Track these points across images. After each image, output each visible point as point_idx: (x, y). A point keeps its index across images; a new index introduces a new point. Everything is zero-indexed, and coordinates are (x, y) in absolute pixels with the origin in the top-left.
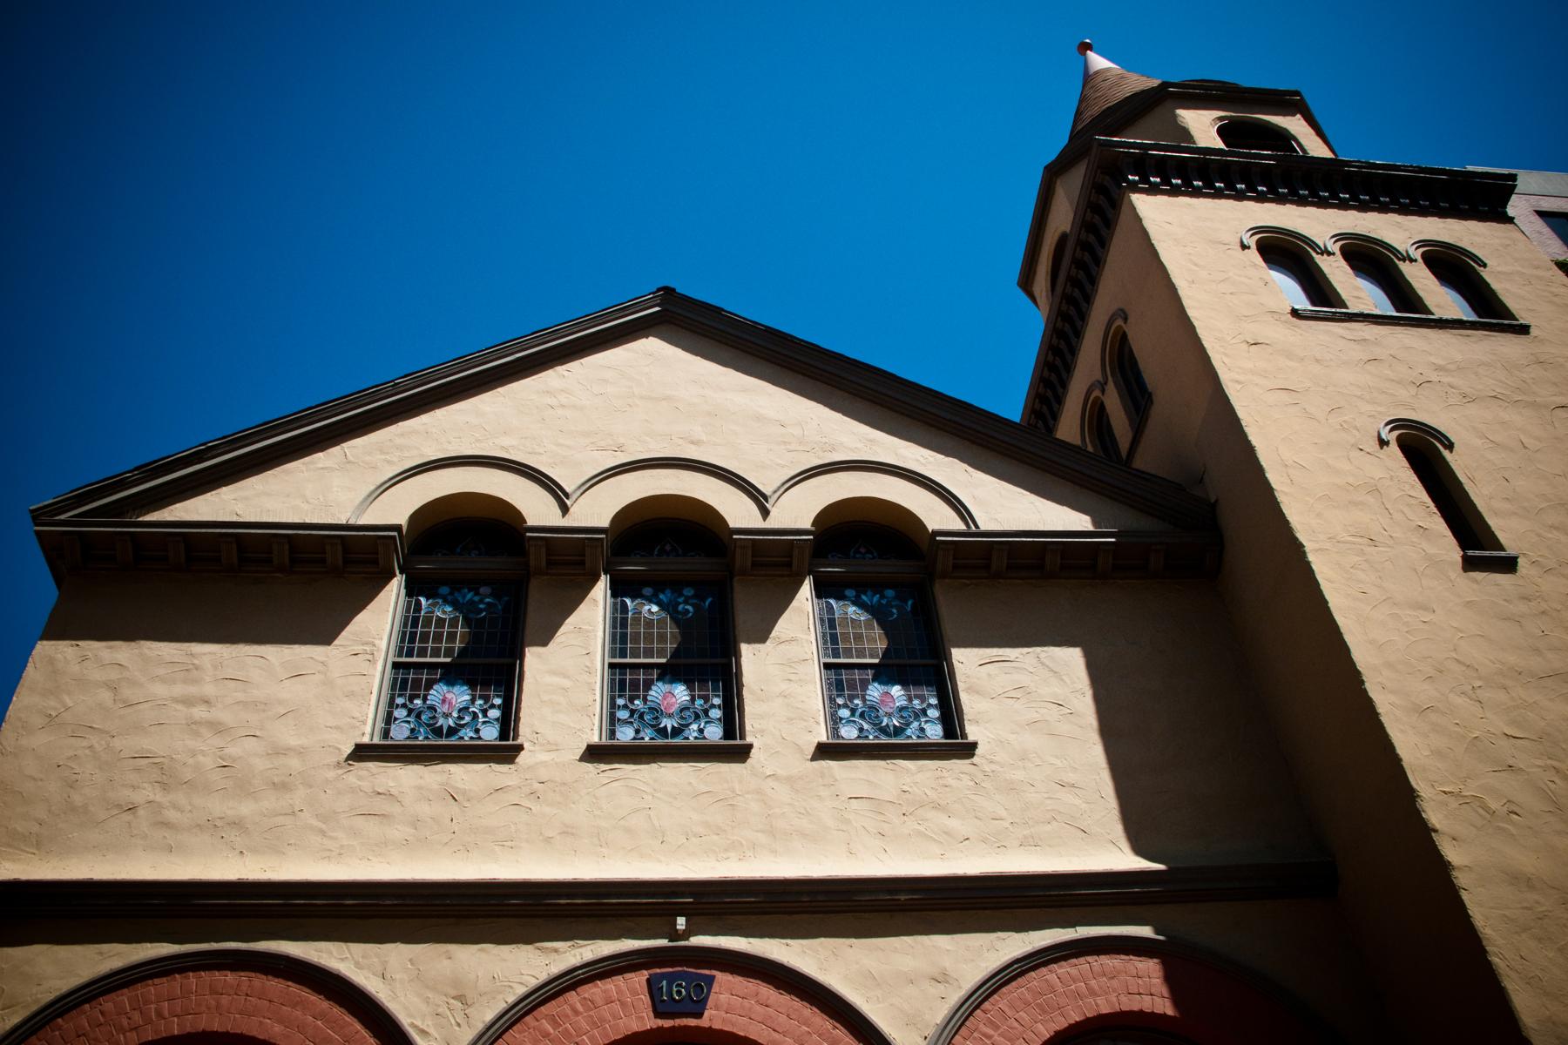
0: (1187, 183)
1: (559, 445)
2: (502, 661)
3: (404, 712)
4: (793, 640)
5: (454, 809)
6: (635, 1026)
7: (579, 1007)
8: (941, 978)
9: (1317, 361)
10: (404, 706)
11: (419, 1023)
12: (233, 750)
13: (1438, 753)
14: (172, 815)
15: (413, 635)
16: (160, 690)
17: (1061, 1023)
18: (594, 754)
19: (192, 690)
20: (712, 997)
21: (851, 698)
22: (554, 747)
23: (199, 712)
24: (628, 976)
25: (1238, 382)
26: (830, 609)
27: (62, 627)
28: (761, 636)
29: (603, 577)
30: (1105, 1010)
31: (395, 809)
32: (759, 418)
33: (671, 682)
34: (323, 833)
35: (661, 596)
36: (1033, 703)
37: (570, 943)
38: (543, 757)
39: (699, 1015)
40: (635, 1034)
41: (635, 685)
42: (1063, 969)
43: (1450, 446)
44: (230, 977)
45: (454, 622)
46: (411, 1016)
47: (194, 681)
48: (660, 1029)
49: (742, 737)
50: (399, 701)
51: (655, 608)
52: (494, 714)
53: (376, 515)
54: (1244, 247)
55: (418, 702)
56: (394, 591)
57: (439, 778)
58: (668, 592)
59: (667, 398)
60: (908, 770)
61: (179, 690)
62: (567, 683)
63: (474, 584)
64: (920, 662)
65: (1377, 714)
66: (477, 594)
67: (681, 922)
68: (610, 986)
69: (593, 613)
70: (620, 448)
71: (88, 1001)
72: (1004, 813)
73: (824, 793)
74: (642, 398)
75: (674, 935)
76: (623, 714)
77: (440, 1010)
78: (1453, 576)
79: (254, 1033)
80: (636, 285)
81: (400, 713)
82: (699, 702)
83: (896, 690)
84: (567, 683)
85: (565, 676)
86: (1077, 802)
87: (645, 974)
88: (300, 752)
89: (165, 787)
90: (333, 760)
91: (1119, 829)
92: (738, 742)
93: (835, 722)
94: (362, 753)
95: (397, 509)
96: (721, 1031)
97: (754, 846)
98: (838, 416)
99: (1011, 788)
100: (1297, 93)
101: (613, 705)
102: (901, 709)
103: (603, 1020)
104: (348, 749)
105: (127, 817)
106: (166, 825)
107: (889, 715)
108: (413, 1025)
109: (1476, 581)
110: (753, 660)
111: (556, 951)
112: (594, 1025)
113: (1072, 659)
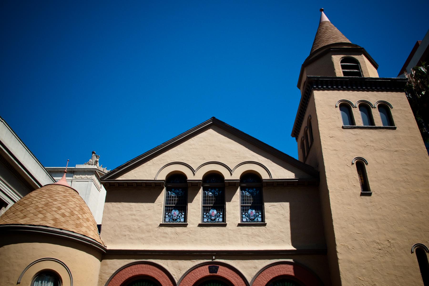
1: (193, 158)
4: (235, 201)
5: (177, 235)
6: (206, 275)
8: (256, 268)
9: (344, 141)
12: (140, 225)
13: (343, 237)
14: (132, 237)
16: (126, 213)
17: (274, 276)
18: (200, 225)
19: (132, 213)
21: (245, 213)
22: (193, 224)
23: (133, 217)
25: (326, 149)
26: (243, 193)
28: (230, 201)
30: (282, 274)
31: (167, 236)
34: (156, 240)
36: (278, 213)
38: (192, 226)
39: (216, 273)
41: (207, 210)
42: (276, 267)
43: (367, 164)
44: (144, 265)
45: (175, 197)
47: (132, 211)
50: (167, 214)
51: (211, 193)
52: (183, 216)
53: (159, 178)
54: (336, 107)
56: (164, 191)
59: (213, 146)
61: (130, 212)
62: (195, 211)
65: (333, 229)
67: (214, 257)
69: (199, 197)
70: (204, 159)
72: (270, 237)
73: (239, 233)
75: (213, 260)
76: (205, 216)
78: (358, 197)
81: (167, 216)
83: (254, 211)
84: (195, 211)
85: (195, 209)
86: (283, 235)
87: (208, 266)
88: (151, 225)
89: (130, 232)
90: (156, 226)
91: (290, 240)
94: (161, 225)
95: (162, 177)
97: (226, 243)
98: (247, 149)
99: (272, 232)
100: (363, 48)
101: (203, 214)
102: (254, 215)
104: (159, 225)
105: (125, 237)
106: (131, 239)
109: (362, 198)
110: (228, 205)
113: (287, 205)
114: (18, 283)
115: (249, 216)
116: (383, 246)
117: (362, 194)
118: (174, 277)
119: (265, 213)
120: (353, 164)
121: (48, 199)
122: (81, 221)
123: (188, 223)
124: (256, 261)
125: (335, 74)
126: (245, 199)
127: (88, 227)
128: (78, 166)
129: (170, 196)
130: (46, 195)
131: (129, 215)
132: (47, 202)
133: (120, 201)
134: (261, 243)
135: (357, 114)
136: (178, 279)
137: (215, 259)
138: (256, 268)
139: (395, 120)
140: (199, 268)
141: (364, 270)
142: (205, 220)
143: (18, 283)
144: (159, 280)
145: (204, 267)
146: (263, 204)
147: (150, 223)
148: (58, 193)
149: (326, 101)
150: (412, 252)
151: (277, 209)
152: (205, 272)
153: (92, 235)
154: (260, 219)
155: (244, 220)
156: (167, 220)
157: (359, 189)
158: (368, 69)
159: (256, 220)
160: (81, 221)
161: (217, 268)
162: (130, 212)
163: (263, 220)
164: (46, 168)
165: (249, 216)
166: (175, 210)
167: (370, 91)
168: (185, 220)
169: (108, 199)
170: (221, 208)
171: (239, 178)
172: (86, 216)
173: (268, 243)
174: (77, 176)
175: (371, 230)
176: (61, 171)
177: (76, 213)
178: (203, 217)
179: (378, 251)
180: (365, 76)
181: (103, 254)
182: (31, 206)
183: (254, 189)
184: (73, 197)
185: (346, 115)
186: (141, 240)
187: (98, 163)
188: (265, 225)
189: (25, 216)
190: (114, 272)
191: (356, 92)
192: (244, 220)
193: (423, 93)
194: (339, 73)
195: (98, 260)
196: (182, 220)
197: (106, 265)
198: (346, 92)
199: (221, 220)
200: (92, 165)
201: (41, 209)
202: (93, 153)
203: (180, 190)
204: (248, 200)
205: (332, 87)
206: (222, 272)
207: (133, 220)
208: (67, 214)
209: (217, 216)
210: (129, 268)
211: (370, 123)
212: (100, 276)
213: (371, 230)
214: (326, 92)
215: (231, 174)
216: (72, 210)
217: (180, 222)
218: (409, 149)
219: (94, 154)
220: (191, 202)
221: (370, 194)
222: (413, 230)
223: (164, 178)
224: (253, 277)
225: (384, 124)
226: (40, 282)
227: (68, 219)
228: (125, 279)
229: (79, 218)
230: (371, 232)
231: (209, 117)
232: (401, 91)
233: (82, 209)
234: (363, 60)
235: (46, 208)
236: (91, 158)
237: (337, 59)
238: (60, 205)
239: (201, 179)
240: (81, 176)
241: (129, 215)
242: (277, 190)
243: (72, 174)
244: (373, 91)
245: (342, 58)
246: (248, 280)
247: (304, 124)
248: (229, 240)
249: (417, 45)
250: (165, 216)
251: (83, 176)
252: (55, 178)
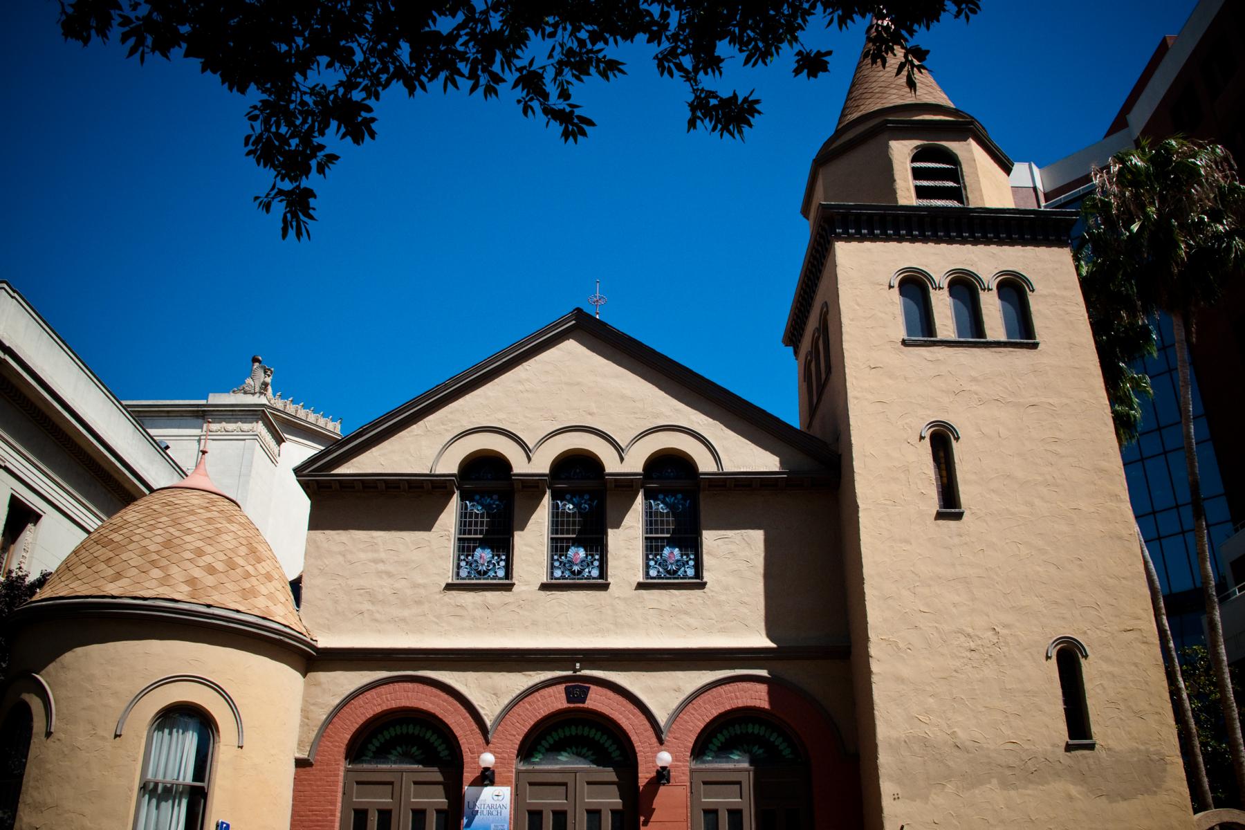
0: (871, 233)
5: (489, 613)
8: (678, 690)
9: (906, 378)
12: (397, 585)
14: (377, 616)
16: (362, 556)
17: (722, 710)
19: (376, 555)
22: (527, 583)
23: (381, 567)
32: (623, 397)
36: (736, 557)
38: (524, 588)
41: (562, 547)
43: (957, 439)
45: (482, 516)
47: (376, 551)
52: (502, 564)
53: (441, 469)
59: (578, 384)
61: (370, 555)
62: (532, 550)
67: (578, 665)
69: (542, 517)
76: (557, 564)
81: (463, 564)
84: (532, 550)
87: (564, 686)
88: (424, 586)
89: (373, 603)
91: (763, 624)
94: (449, 587)
95: (449, 465)
98: (662, 393)
99: (719, 604)
105: (360, 617)
106: (376, 620)
113: (758, 536)
114: (116, 736)
115: (663, 563)
116: (979, 642)
117: (940, 516)
118: (482, 712)
119: (705, 557)
120: (922, 438)
121: (171, 530)
122: (255, 582)
123: (514, 581)
124: (680, 674)
125: (894, 192)
126: (656, 521)
127: (270, 597)
128: (216, 399)
129: (471, 514)
130: (164, 519)
131: (370, 561)
132: (168, 536)
134: (692, 629)
135: (943, 306)
136: (493, 718)
138: (678, 690)
139: (1038, 323)
140: (543, 692)
141: (931, 700)
142: (558, 573)
143: (116, 736)
146: (700, 535)
147: (421, 581)
148: (192, 512)
149: (866, 272)
150: (1048, 658)
151: (733, 547)
152: (556, 700)
153: (282, 613)
154: (691, 572)
155: (653, 573)
156: (464, 573)
157: (933, 503)
158: (982, 180)
159: (680, 573)
160: (255, 582)
161: (585, 691)
162: (370, 555)
163: (698, 572)
164: (124, 403)
165: (663, 563)
166: (483, 548)
167: (981, 243)
168: (509, 574)
169: (316, 523)
170: (596, 544)
171: (640, 470)
172: (264, 567)
173: (709, 630)
174: (214, 427)
175: (955, 605)
176: (168, 412)
177: (240, 561)
178: (552, 567)
179: (969, 654)
180: (973, 203)
181: (311, 659)
182: (131, 547)
183: (679, 496)
184: (230, 521)
185: (914, 308)
186: (401, 623)
187: (270, 388)
188: (702, 586)
189: (118, 576)
190: (337, 701)
191: (943, 246)
192: (653, 573)
193: (1135, 228)
194: (906, 193)
195: (298, 675)
196: (501, 573)
197: (318, 684)
198: (918, 245)
199: (595, 573)
200: (254, 394)
201: (155, 557)
202: (255, 360)
203: (495, 497)
204: (662, 522)
205: (884, 232)
206: (597, 700)
207: (379, 573)
208: (220, 566)
209: (585, 563)
210: (373, 692)
211: (973, 331)
212: (305, 713)
213: (955, 605)
214: (867, 244)
215: (622, 459)
216: (230, 554)
217: (589, 578)
218: (1065, 401)
219: (257, 364)
221: (959, 516)
222: (1056, 603)
223: (454, 469)
224: (670, 712)
225: (1009, 336)
226: (167, 731)
227: (223, 578)
228: (364, 719)
229: (247, 576)
230: (954, 610)
231: (567, 309)
232: (1060, 243)
233: (253, 551)
234: (971, 154)
235: (166, 552)
236: (250, 374)
237: (902, 151)
238: (200, 544)
239: (547, 471)
240: (224, 424)
241: (370, 561)
242: (737, 498)
243: (200, 421)
244: (988, 242)
245: (916, 148)
247: (813, 323)
248: (616, 624)
249: (1163, 48)
251: (230, 426)
252: (152, 432)
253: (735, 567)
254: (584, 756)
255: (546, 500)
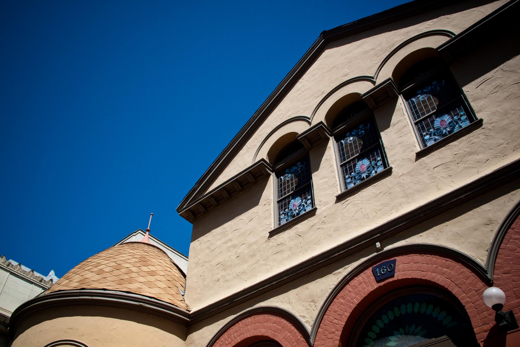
2: (376, 144)
3: (283, 215)
4: (399, 121)
6: (371, 289)
7: (351, 290)
10: (349, 177)
11: (302, 314)
14: (228, 277)
15: (281, 190)
16: (219, 243)
19: (227, 238)
20: (396, 267)
21: (428, 130)
23: (229, 244)
24: (365, 272)
27: (195, 236)
29: (331, 138)
33: (362, 160)
34: (266, 264)
35: (425, 90)
37: (344, 268)
38: (324, 208)
39: (393, 276)
40: (372, 292)
44: (249, 320)
46: (299, 313)
48: (380, 287)
49: (389, 166)
50: (347, 177)
55: (287, 210)
57: (294, 231)
58: (355, 131)
60: (455, 145)
61: (223, 240)
62: (326, 180)
63: (295, 164)
64: (453, 101)
66: (297, 166)
67: (378, 245)
68: (360, 278)
69: (332, 152)
71: (217, 339)
72: (502, 141)
74: (326, 72)
75: (378, 250)
77: (307, 308)
79: (259, 334)
80: (314, 36)
82: (373, 162)
85: (325, 178)
88: (255, 243)
89: (225, 270)
92: (388, 168)
93: (424, 142)
96: (402, 279)
102: (450, 123)
103: (359, 291)
105: (218, 283)
106: (227, 281)
107: (445, 128)
108: (300, 316)
110: (387, 137)
111: (340, 273)
112: (357, 294)
119: (472, 104)
122: (133, 275)
124: (486, 207)
131: (223, 244)
133: (209, 231)
136: (312, 323)
137: (382, 247)
144: (276, 339)
145: (362, 274)
146: (462, 92)
147: (253, 240)
152: (367, 284)
203: (299, 164)
206: (406, 268)
210: (225, 335)
220: (317, 169)
224: (489, 247)
241: (223, 244)
246: (478, 261)
250: (280, 218)
253: (506, 94)
254: (414, 334)
255: (332, 144)
